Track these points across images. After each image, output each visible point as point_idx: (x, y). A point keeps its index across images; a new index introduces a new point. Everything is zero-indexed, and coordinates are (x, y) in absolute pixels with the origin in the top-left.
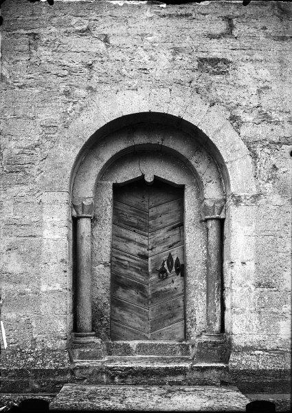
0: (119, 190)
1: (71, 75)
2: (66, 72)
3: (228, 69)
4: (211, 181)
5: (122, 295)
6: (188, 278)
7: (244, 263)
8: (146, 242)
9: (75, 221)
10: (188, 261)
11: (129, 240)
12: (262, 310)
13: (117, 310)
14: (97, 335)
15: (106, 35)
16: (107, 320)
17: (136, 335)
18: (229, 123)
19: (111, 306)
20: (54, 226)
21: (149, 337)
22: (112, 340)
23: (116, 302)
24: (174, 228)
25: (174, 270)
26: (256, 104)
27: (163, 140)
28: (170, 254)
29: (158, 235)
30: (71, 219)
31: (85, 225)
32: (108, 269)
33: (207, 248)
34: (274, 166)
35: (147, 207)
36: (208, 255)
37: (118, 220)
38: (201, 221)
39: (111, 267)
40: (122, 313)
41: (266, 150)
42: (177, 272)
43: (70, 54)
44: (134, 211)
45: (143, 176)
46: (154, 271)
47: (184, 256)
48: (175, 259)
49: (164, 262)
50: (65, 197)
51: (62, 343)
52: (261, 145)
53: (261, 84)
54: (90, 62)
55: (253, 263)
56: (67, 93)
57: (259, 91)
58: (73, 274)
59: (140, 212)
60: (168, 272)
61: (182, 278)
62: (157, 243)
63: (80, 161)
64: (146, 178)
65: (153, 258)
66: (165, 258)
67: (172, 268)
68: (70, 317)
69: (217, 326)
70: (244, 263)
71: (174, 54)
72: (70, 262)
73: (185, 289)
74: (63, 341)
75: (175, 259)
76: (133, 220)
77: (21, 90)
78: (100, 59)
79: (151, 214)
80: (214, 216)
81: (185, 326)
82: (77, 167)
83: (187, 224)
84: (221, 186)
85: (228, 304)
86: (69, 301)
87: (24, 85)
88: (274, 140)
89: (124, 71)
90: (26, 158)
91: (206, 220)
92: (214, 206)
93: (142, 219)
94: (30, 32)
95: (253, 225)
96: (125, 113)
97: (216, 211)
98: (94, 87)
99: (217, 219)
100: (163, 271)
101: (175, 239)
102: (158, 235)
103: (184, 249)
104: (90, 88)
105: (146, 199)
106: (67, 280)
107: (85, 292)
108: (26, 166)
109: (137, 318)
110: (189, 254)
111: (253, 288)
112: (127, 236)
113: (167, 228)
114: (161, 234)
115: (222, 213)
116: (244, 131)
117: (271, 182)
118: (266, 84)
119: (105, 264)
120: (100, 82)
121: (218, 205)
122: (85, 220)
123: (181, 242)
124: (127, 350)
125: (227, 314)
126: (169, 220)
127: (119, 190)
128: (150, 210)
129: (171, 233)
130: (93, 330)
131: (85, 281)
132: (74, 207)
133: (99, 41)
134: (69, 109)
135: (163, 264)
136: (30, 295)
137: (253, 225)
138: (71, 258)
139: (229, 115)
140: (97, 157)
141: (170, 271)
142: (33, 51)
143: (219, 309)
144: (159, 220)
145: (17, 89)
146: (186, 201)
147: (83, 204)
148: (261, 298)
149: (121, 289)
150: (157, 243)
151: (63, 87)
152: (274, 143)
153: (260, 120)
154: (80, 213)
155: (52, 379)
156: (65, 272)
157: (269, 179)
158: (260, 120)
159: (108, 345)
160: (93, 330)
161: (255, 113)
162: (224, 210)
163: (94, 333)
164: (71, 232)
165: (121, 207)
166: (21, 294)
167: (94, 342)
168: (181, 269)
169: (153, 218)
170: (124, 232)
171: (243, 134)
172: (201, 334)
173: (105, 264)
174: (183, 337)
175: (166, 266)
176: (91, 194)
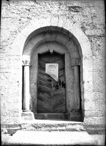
0: (40, 56)
6: (67, 89)
21: (52, 112)
25: (61, 86)
33: (74, 77)
34: (99, 45)
48: (62, 81)
60: (59, 86)
67: (61, 85)
75: (62, 81)
81: (66, 107)
103: (65, 78)
127: (40, 56)
141: (60, 86)
143: (79, 100)
146: (66, 61)
149: (41, 93)
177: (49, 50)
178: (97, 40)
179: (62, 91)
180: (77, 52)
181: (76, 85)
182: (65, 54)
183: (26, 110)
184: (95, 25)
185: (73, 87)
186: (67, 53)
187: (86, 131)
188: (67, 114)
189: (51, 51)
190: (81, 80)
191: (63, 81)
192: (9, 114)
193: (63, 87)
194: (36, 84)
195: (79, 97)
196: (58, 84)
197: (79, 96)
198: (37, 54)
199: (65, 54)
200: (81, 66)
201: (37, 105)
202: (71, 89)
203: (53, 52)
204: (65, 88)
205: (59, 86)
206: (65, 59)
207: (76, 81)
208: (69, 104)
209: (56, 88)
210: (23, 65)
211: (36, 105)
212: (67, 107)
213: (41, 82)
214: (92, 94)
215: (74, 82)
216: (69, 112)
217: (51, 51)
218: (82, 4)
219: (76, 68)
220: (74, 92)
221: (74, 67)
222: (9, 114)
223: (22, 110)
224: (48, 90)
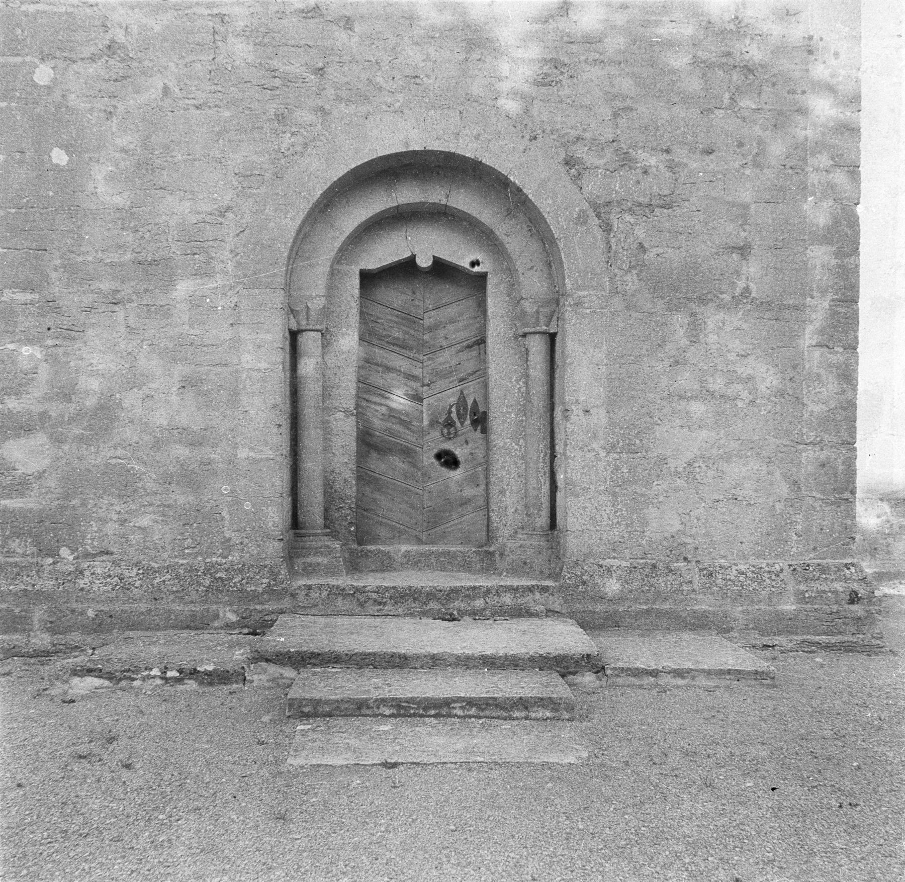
0: (368, 279)
1: (288, 86)
2: (277, 82)
3: (561, 77)
4: (532, 268)
5: (377, 464)
6: (493, 437)
7: (587, 412)
8: (418, 372)
9: (294, 336)
10: (493, 405)
11: (389, 369)
12: (617, 489)
13: (367, 490)
14: (334, 535)
15: (349, 18)
16: (350, 508)
17: (398, 534)
18: (562, 169)
19: (357, 485)
20: (259, 347)
21: (424, 538)
22: (360, 544)
23: (364, 477)
24: (469, 347)
25: (468, 422)
26: (610, 137)
27: (447, 197)
28: (462, 393)
29: (441, 359)
30: (287, 335)
31: (310, 342)
32: (352, 420)
33: (526, 384)
34: (641, 245)
35: (421, 311)
36: (527, 395)
37: (368, 336)
38: (516, 337)
39: (357, 416)
40: (376, 496)
41: (628, 217)
42: (475, 423)
43: (286, 49)
44: (397, 316)
45: (413, 257)
46: (433, 423)
47: (486, 397)
48: (470, 402)
49: (451, 407)
50: (278, 299)
51: (274, 548)
52: (619, 210)
53: (619, 104)
54: (320, 65)
55: (602, 412)
56: (281, 118)
57: (615, 115)
58: (291, 430)
59: (409, 319)
60: (458, 424)
61: (484, 435)
62: (439, 375)
63: (302, 233)
64: (418, 260)
65: (431, 400)
66: (453, 400)
67: (465, 419)
68: (287, 502)
69: (543, 520)
70: (587, 412)
71: (469, 50)
72: (287, 408)
73: (487, 455)
74: (276, 544)
75: (470, 402)
76: (396, 333)
77: (198, 112)
78: (337, 59)
79: (427, 322)
80: (538, 329)
81: (489, 518)
82: (298, 242)
83: (490, 341)
84: (550, 276)
85: (560, 477)
86: (286, 475)
87: (205, 104)
88: (641, 200)
89: (379, 79)
90: (210, 231)
91: (524, 335)
92: (538, 312)
93: (412, 332)
94: (215, 11)
95: (605, 348)
96: (382, 153)
97: (543, 320)
98: (327, 107)
99: (544, 333)
100: (449, 424)
101: (470, 366)
102: (441, 359)
103: (486, 386)
104: (322, 109)
105: (418, 295)
106: (280, 439)
107: (312, 466)
108: (211, 243)
109: (404, 506)
110: (495, 394)
111: (603, 454)
112: (385, 361)
113: (458, 347)
114: (446, 358)
115: (554, 323)
116: (592, 185)
117: (634, 272)
118: (629, 102)
119: (346, 412)
120: (338, 99)
121: (546, 310)
122: (313, 334)
123: (481, 373)
124: (386, 564)
125: (559, 496)
126: (461, 333)
127: (368, 279)
128: (425, 315)
129: (464, 356)
130: (326, 527)
131: (312, 438)
132: (292, 311)
133: (336, 28)
134: (284, 146)
135: (450, 412)
136: (220, 465)
137: (605, 348)
138: (288, 402)
139: (563, 155)
140: (332, 226)
141: (462, 424)
142: (220, 44)
143: (546, 488)
144: (441, 333)
145: (193, 110)
146: (490, 301)
147: (307, 307)
148: (617, 469)
149: (374, 455)
150: (439, 375)
151: (272, 109)
152: (640, 205)
153: (618, 164)
154: (304, 322)
155: (258, 607)
156: (280, 426)
157: (634, 267)
158: (618, 164)
159: (352, 552)
160: (326, 527)
161: (609, 152)
162: (555, 318)
163: (328, 530)
164: (288, 357)
165: (376, 311)
166: (202, 463)
167: (328, 547)
168: (481, 421)
169: (431, 329)
170: (380, 354)
171: (587, 189)
172: (516, 532)
173: (346, 412)
174: (484, 539)
175: (454, 416)
176: (321, 290)
177: (415, 256)
178: (632, 221)
179: (470, 445)
180: (545, 269)
181: (537, 423)
182: (487, 272)
183: (311, 531)
184: (631, 150)
185: (520, 433)
186: (496, 272)
187: (571, 615)
188: (492, 549)
189: (424, 262)
190: (557, 400)
191: (475, 401)
192: (240, 547)
193: (475, 430)
194: (352, 415)
195: (548, 475)
196: (454, 416)
197: (547, 469)
198: (358, 273)
199: (489, 276)
200: (558, 339)
201: (358, 506)
202: (515, 438)
203: (430, 263)
204: (484, 431)
205: (458, 424)
206: (489, 300)
207: (539, 403)
208: (503, 505)
209: (445, 431)
210: (294, 327)
211: (353, 506)
212: (494, 517)
213: (375, 403)
214: (602, 464)
215: (524, 405)
216: (500, 540)
217: (424, 262)
218: (572, 46)
219: (537, 346)
220: (525, 451)
221: (529, 337)
222: (240, 547)
223: (293, 531)
224: (408, 441)
